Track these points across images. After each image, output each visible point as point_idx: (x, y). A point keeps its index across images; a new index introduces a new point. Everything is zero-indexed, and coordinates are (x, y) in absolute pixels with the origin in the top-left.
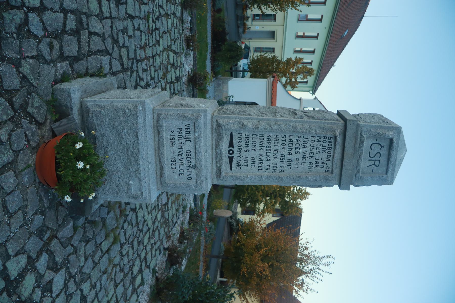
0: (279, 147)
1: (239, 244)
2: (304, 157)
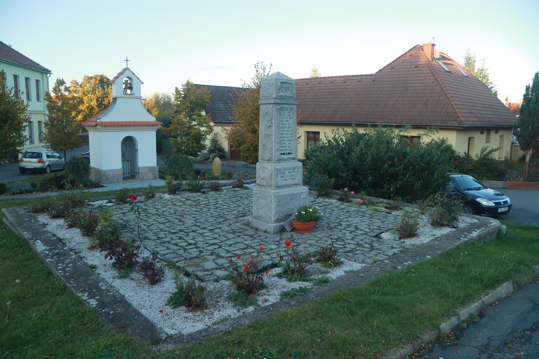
0: (284, 132)
1: (252, 149)
2: (287, 121)
